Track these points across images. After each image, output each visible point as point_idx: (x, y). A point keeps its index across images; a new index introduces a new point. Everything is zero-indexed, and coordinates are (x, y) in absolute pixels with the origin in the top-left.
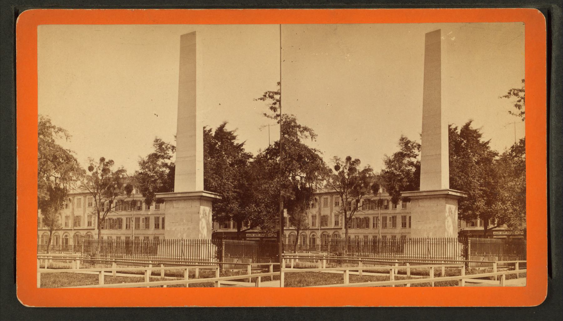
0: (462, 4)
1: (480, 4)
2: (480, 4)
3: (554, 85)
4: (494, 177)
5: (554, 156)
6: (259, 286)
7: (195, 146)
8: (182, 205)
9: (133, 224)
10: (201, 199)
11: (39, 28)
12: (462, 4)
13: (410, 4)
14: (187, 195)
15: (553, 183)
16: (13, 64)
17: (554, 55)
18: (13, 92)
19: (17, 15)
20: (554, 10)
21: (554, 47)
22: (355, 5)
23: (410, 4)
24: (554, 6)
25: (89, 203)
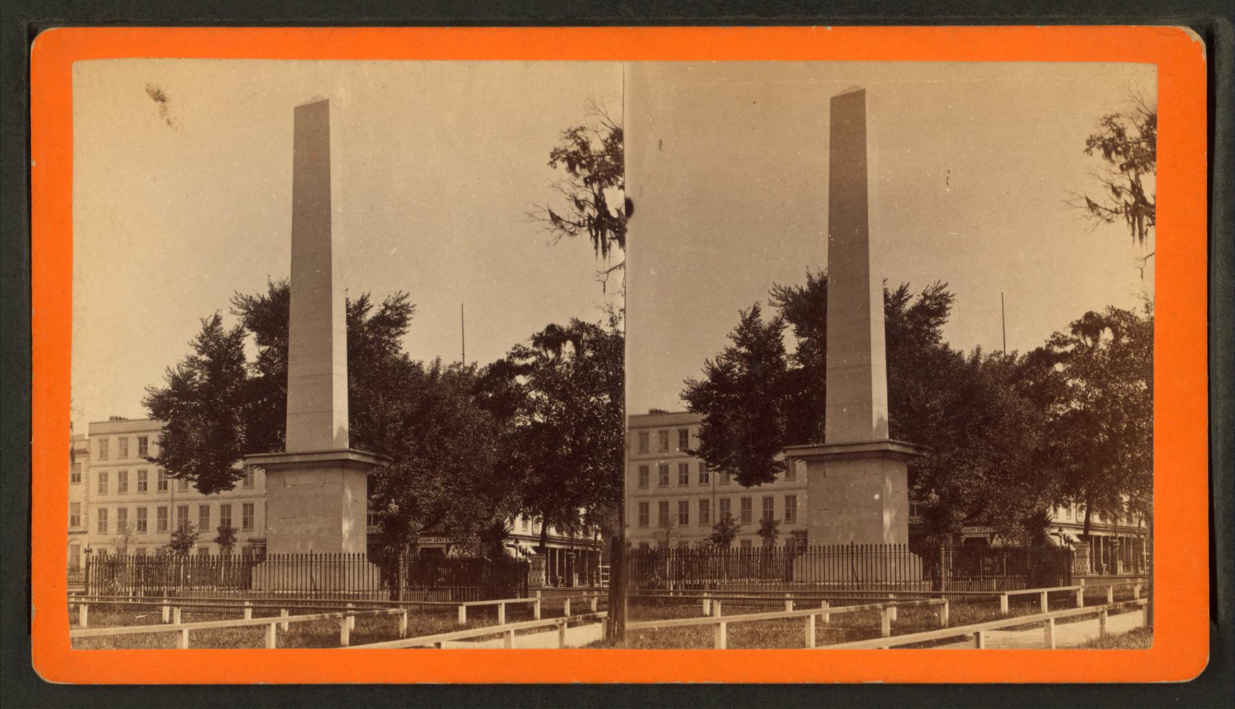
0: (1017, 16)
1: (1057, 16)
2: (1057, 16)
3: (1221, 195)
4: (1066, 400)
5: (1220, 353)
6: (514, 646)
7: (330, 350)
8: (306, 479)
9: (674, 509)
10: (344, 465)
11: (76, 65)
12: (1017, 16)
13: (902, 16)
14: (316, 458)
15: (1220, 412)
16: (24, 150)
17: (1219, 127)
18: (25, 212)
19: (31, 37)
20: (1221, 30)
21: (1220, 111)
22: (782, 17)
23: (902, 16)
24: (1219, 20)
25: (73, 476)
